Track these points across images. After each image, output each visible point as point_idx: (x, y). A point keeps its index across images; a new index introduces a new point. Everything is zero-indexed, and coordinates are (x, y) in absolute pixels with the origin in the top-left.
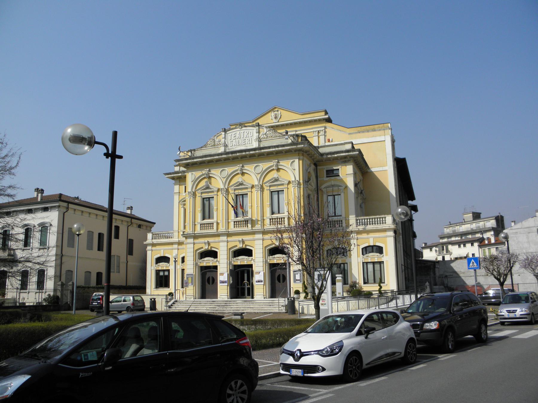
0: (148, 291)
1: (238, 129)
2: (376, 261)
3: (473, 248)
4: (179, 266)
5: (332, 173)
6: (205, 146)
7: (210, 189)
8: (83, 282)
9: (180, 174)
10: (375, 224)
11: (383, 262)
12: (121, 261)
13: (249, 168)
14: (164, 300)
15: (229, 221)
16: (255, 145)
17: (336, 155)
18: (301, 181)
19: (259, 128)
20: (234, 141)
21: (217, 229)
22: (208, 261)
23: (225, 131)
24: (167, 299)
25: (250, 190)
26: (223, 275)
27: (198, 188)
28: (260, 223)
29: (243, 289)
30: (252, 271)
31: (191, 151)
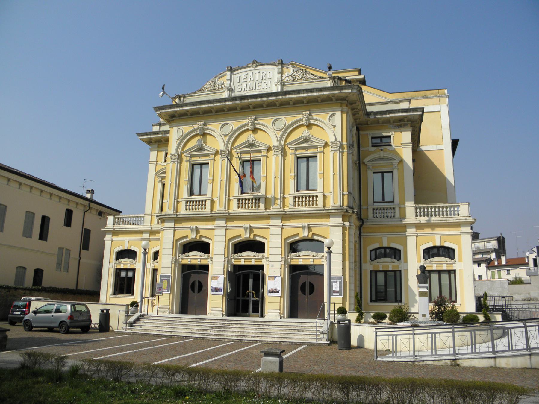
0: (102, 298)
1: (251, 68)
2: (445, 269)
3: (479, 269)
4: (150, 265)
5: (384, 142)
6: (201, 90)
7: (205, 150)
8: (14, 280)
9: (160, 135)
10: (439, 215)
11: (455, 271)
12: (72, 256)
13: (266, 122)
14: (123, 314)
15: (231, 198)
16: (276, 89)
17: (388, 116)
18: (345, 143)
19: (282, 67)
20: (245, 84)
21: (212, 209)
22: (195, 258)
23: (231, 70)
24: (127, 311)
25: (264, 153)
26: (217, 279)
27: (186, 149)
28: (278, 202)
29: (246, 303)
30: (263, 275)
31: (179, 97)
